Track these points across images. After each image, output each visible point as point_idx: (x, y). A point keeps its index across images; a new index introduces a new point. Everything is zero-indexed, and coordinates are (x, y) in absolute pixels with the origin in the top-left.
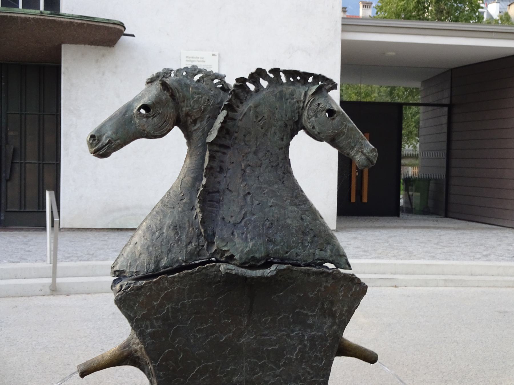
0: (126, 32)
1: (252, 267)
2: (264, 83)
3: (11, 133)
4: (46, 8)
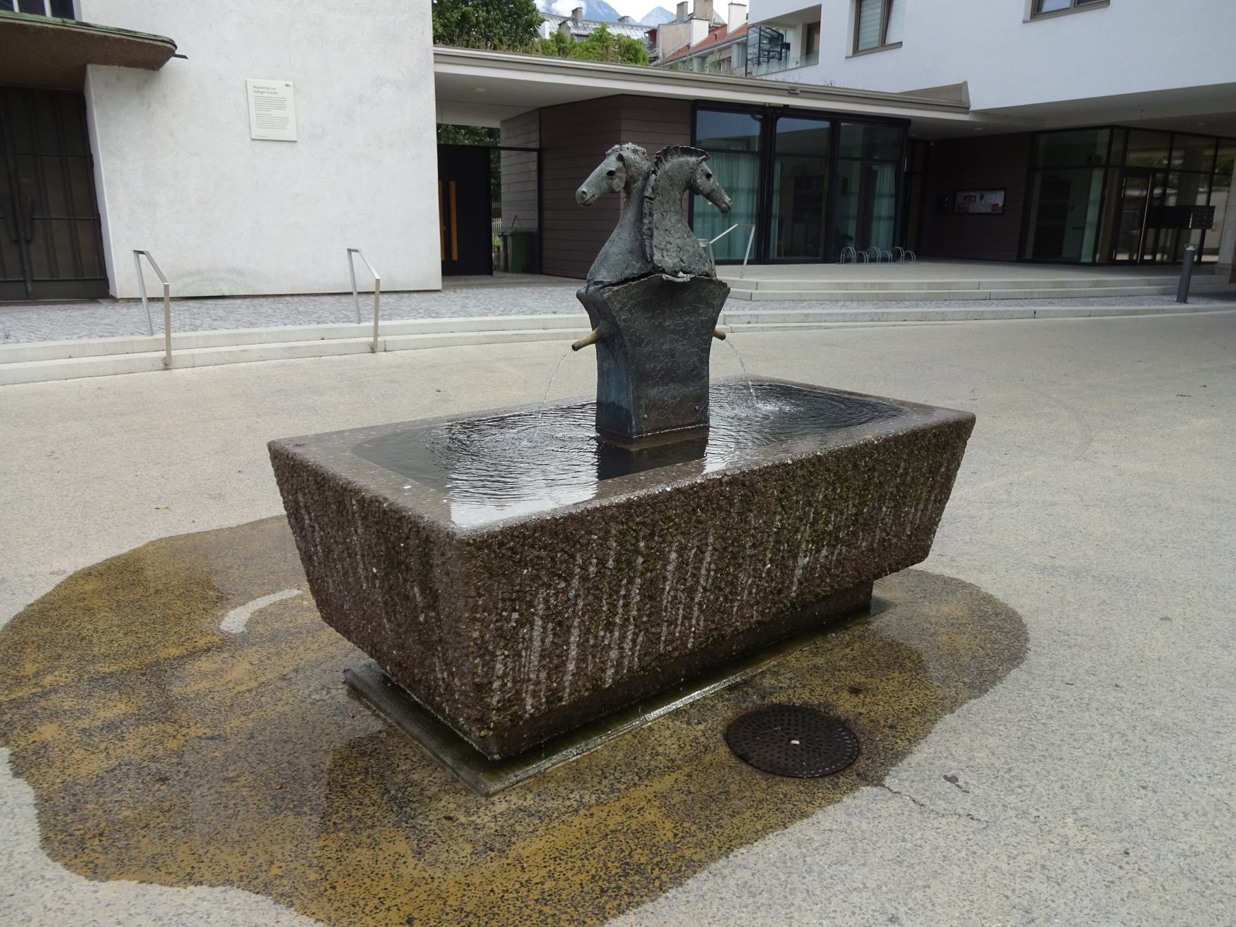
0: (177, 52)
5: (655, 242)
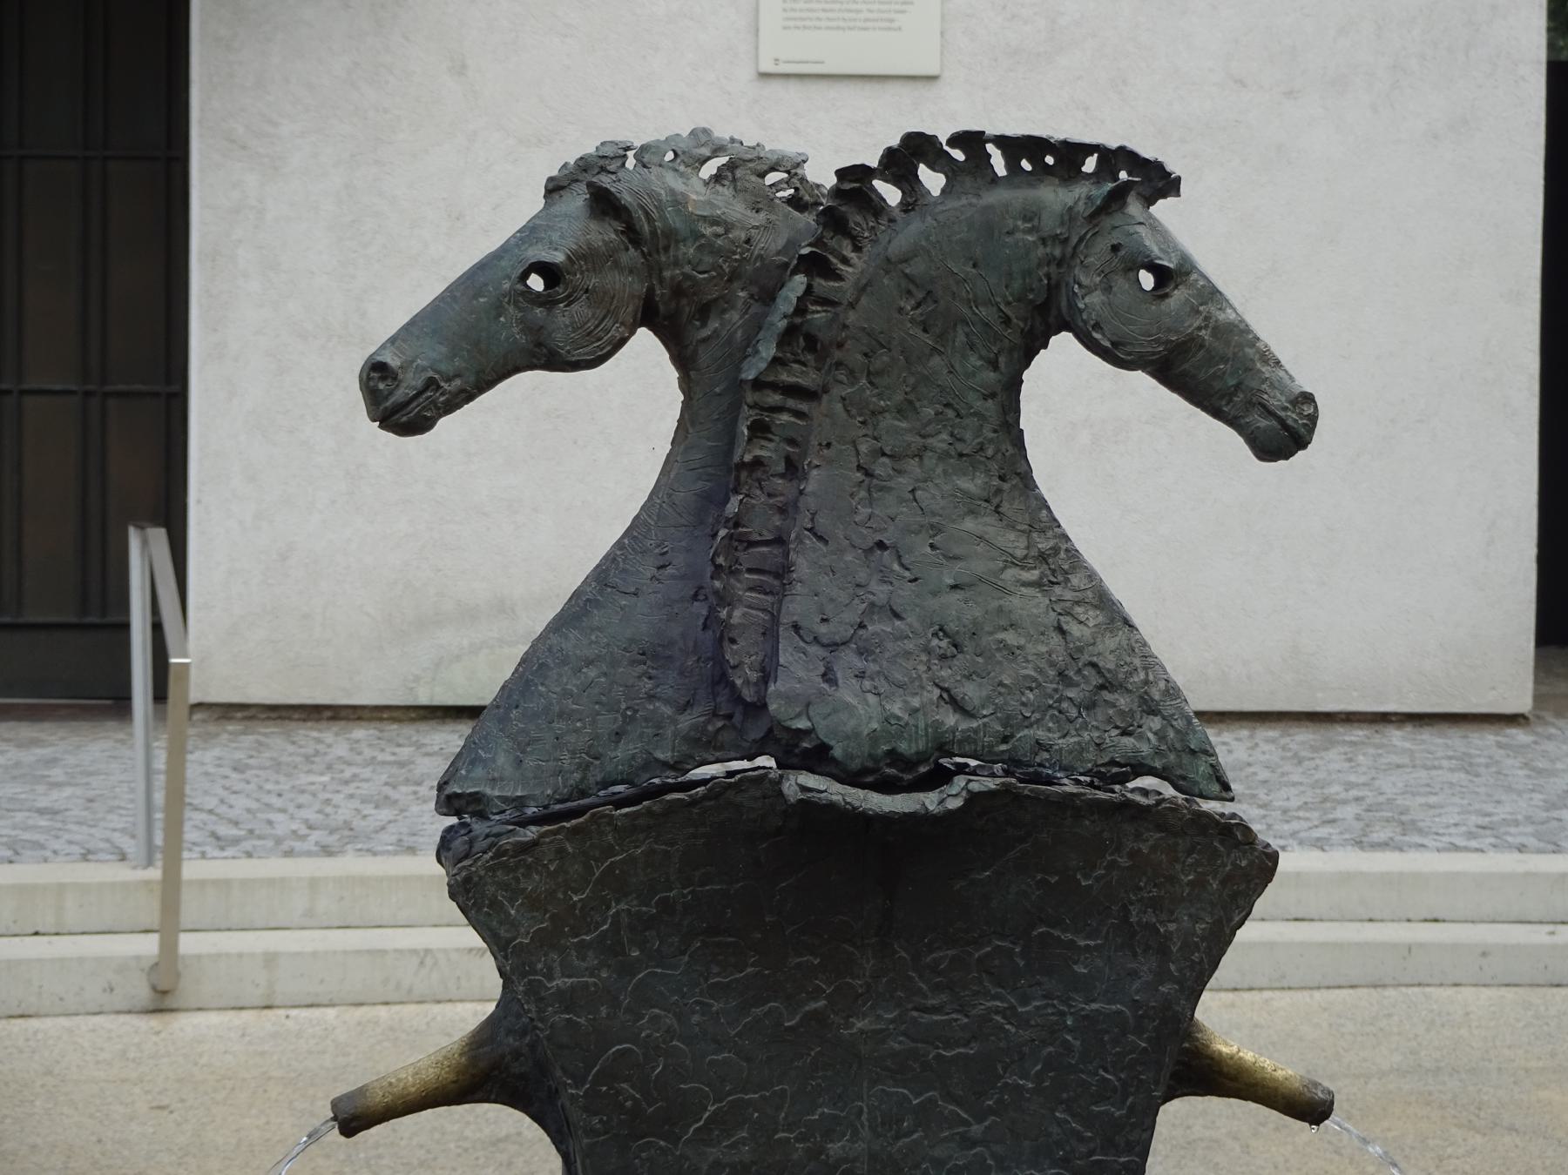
5: (797, 607)
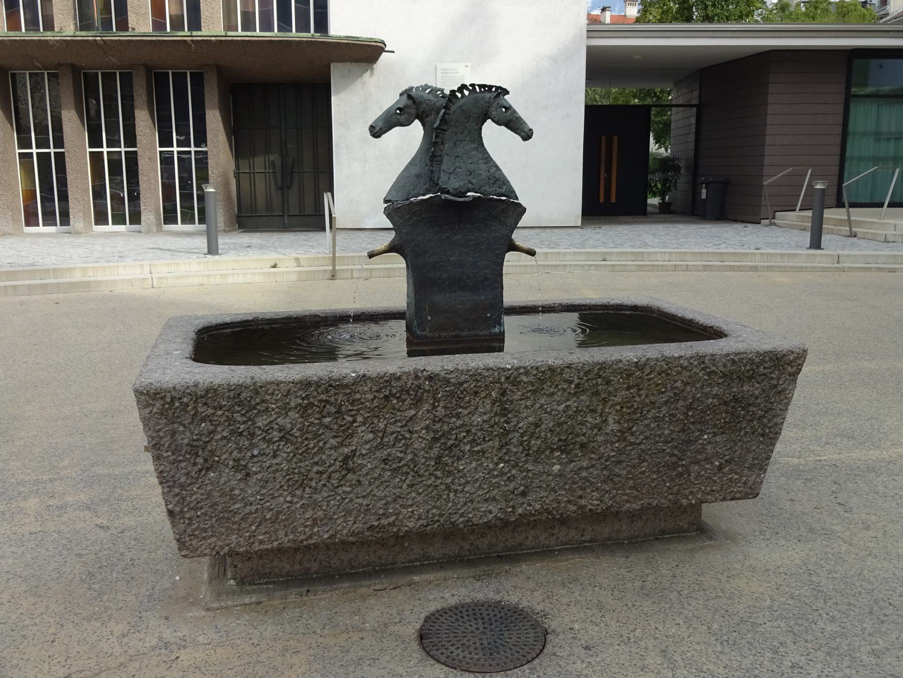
1: (459, 197)
2: (466, 93)
3: (289, 146)
4: (315, 32)
